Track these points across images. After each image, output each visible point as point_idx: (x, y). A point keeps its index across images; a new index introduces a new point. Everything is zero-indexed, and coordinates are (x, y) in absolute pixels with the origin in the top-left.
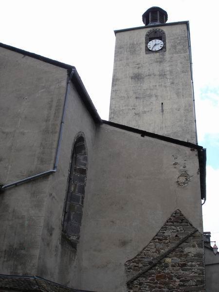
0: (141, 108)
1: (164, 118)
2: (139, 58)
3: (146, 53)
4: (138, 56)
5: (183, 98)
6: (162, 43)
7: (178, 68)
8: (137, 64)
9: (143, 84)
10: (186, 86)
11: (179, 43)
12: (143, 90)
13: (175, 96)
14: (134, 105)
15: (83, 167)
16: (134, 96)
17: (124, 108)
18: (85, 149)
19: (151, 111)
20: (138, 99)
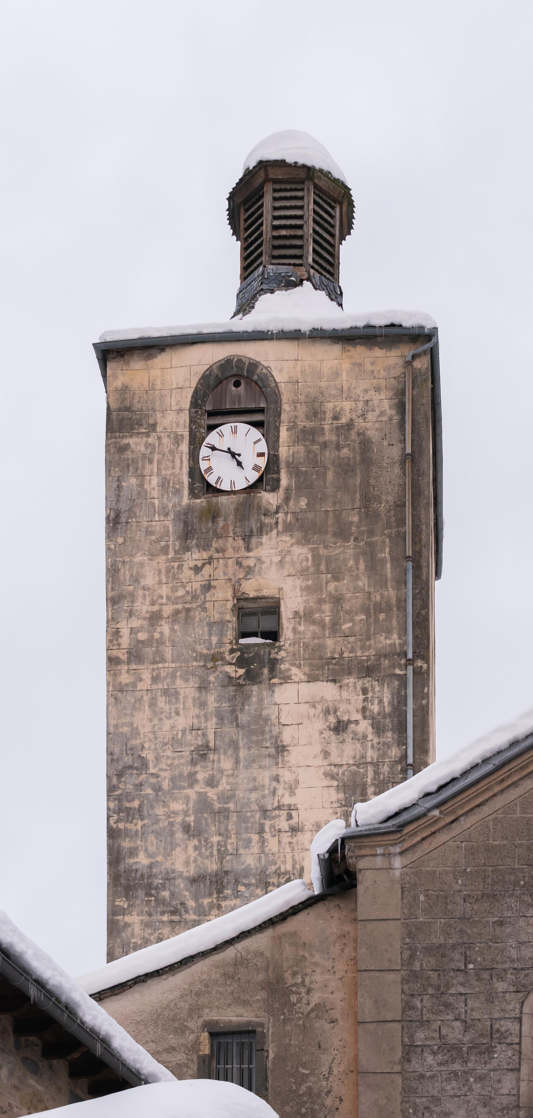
6: (262, 446)
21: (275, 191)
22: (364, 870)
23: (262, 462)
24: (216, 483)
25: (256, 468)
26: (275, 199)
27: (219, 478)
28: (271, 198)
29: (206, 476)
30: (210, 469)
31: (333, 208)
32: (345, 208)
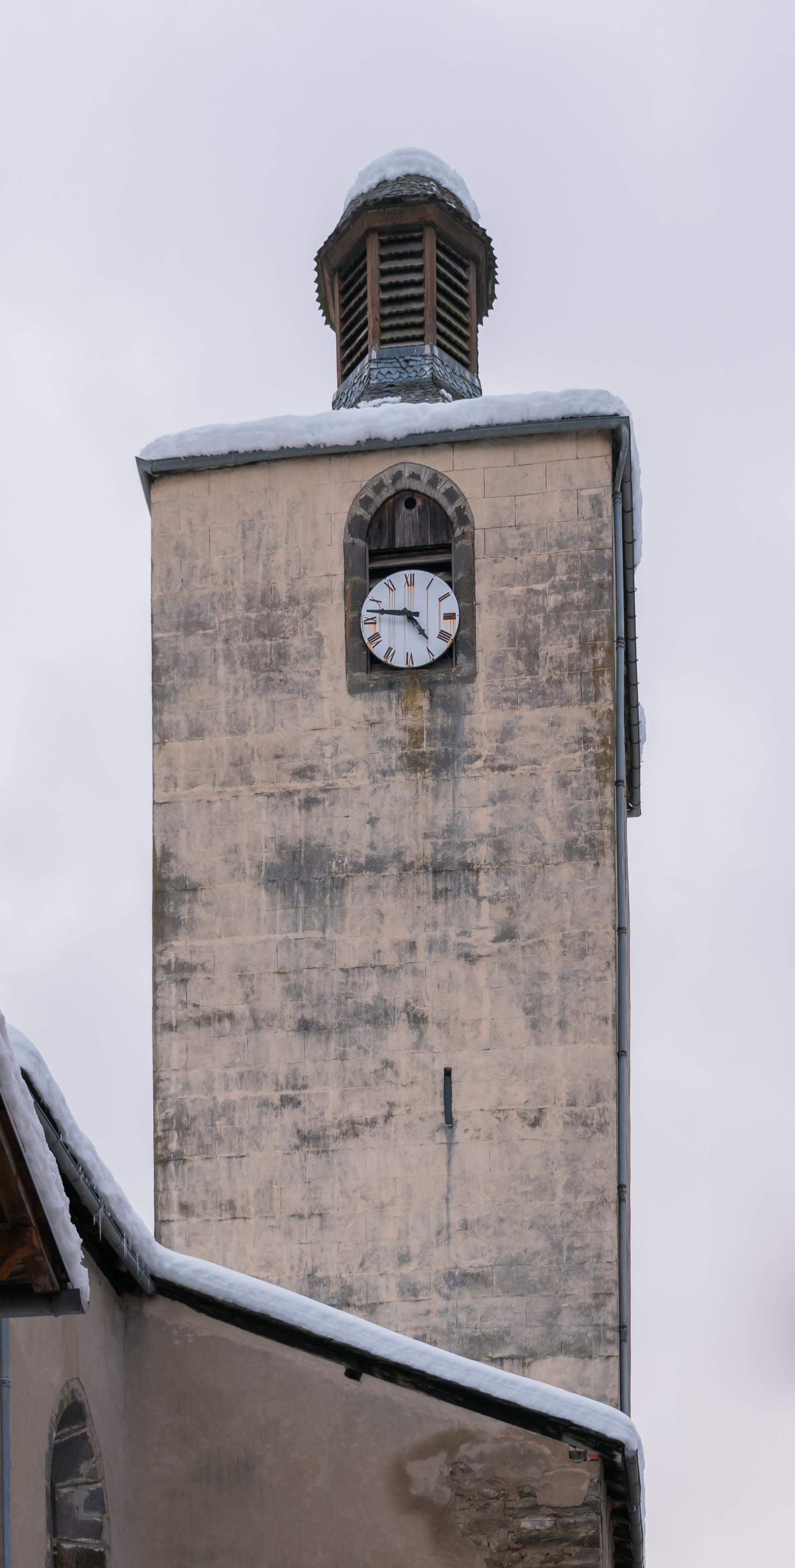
0: (333, 1093)
1: (456, 1172)
2: (307, 722)
3: (354, 689)
4: (300, 702)
5: (563, 1041)
6: (452, 605)
7: (542, 823)
8: (301, 774)
9: (341, 931)
10: (583, 953)
11: (559, 610)
12: (338, 977)
13: (520, 1022)
14: (296, 1082)
15: (86, 1542)
16: (290, 1012)
17: (236, 1094)
18: (89, 1455)
19: (388, 1116)
20: (312, 1038)
21: (383, 244)
22: (450, 1144)
23: (451, 627)
24: (386, 656)
25: (443, 635)
26: (383, 259)
27: (390, 649)
28: (377, 258)
29: (370, 646)
30: (376, 637)
31: (465, 267)
32: (483, 269)
